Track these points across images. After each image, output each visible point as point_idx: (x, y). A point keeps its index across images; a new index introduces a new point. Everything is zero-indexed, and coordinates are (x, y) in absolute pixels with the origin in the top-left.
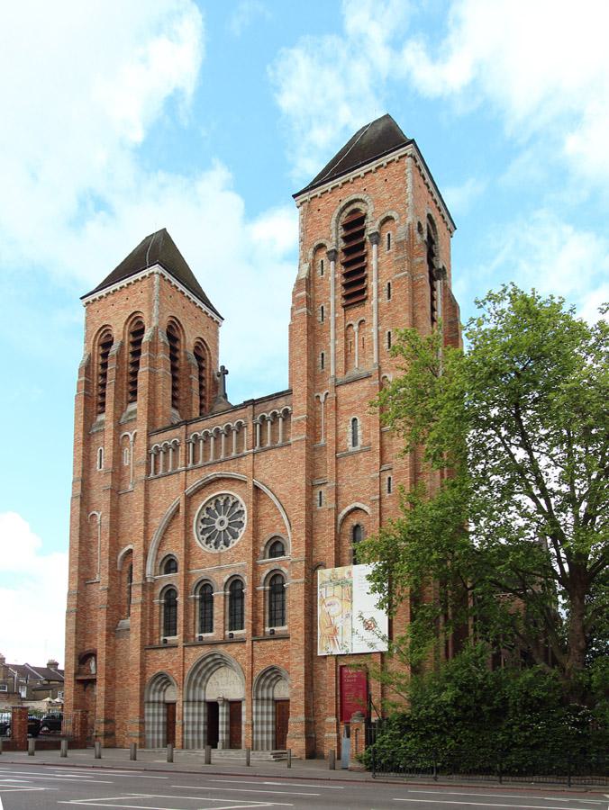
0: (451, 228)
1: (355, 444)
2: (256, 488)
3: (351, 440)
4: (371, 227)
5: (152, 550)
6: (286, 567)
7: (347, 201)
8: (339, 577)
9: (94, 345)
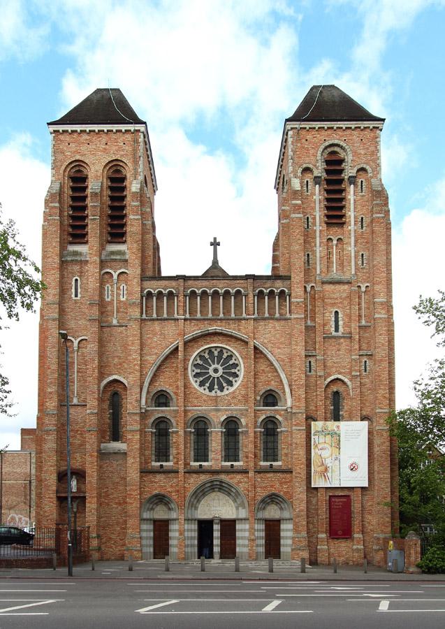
1: (337, 330)
2: (256, 348)
3: (333, 326)
4: (349, 171)
5: (146, 384)
6: (280, 415)
7: (331, 142)
8: (329, 429)
9: (64, 175)
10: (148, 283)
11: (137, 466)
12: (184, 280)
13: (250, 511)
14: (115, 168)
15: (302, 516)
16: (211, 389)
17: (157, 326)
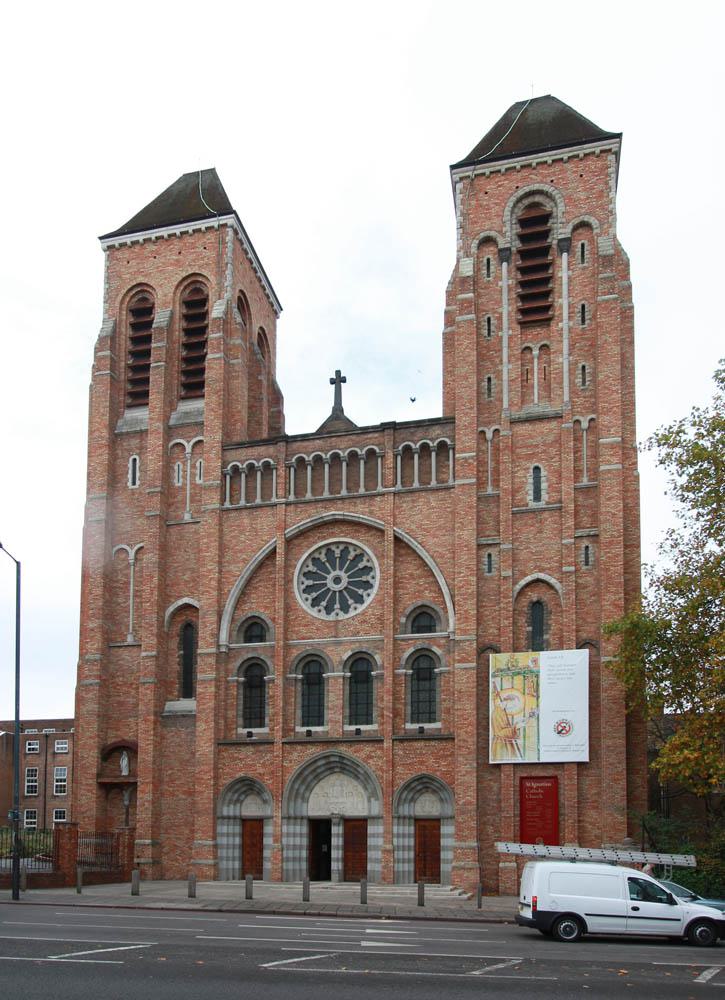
4: (560, 230)
6: (439, 646)
10: (233, 453)
11: (210, 734)
13: (386, 804)
15: (470, 811)
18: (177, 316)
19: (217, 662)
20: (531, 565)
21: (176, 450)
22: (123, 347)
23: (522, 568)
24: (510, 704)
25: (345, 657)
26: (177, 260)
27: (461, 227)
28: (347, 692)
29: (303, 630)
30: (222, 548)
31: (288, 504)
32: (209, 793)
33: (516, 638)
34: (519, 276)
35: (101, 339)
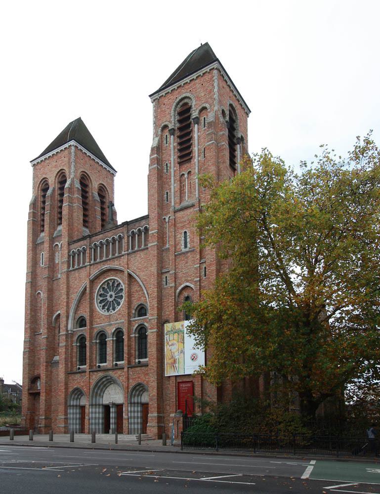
0: (247, 111)
3: (183, 244)
4: (195, 114)
5: (71, 314)
6: (147, 322)
7: (180, 98)
10: (73, 245)
11: (63, 370)
12: (90, 238)
14: (45, 183)
16: (108, 310)
17: (77, 274)
18: (57, 188)
19: (66, 338)
20: (183, 279)
21: (56, 247)
22: (39, 206)
23: (180, 281)
24: (172, 347)
25: (113, 331)
26: (56, 165)
27: (155, 123)
28: (115, 347)
29: (98, 320)
30: (68, 287)
31: (91, 265)
32: (63, 395)
33: (176, 313)
34: (179, 141)
35: (152, 149)
